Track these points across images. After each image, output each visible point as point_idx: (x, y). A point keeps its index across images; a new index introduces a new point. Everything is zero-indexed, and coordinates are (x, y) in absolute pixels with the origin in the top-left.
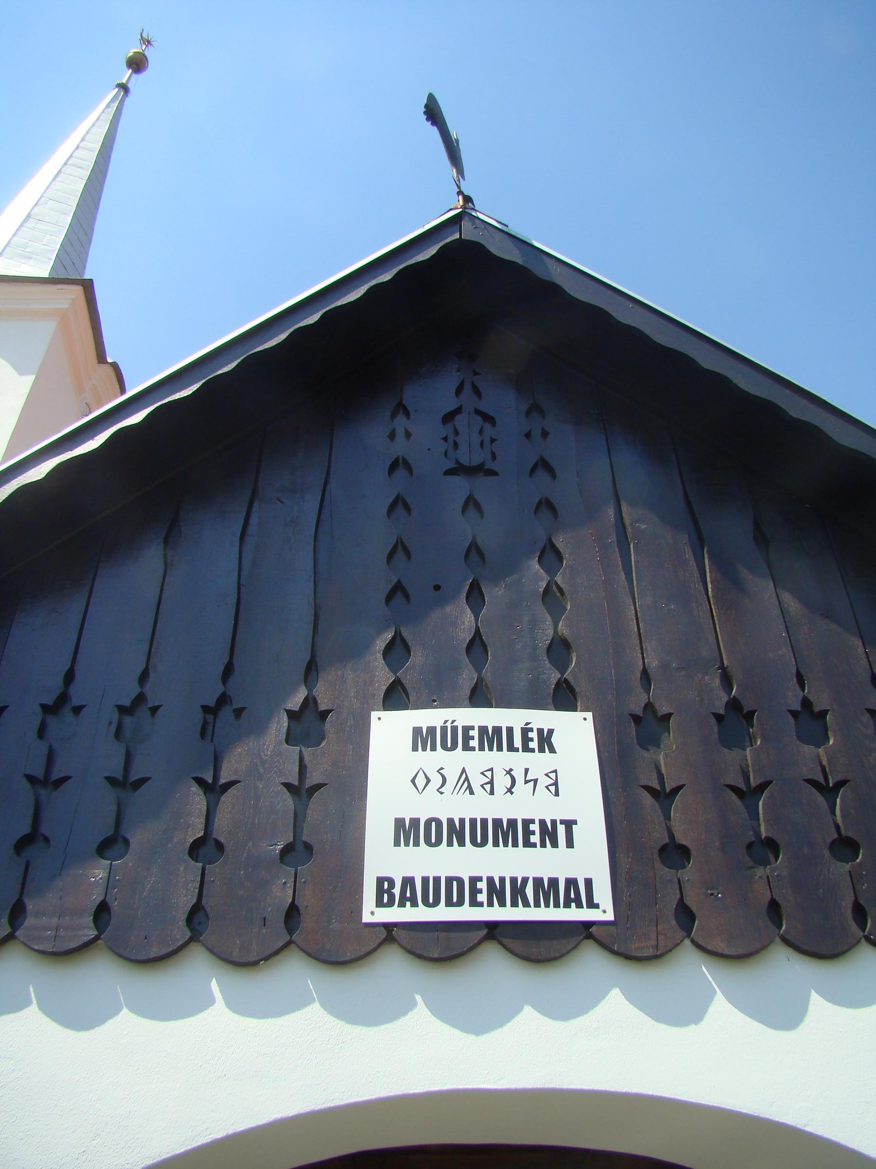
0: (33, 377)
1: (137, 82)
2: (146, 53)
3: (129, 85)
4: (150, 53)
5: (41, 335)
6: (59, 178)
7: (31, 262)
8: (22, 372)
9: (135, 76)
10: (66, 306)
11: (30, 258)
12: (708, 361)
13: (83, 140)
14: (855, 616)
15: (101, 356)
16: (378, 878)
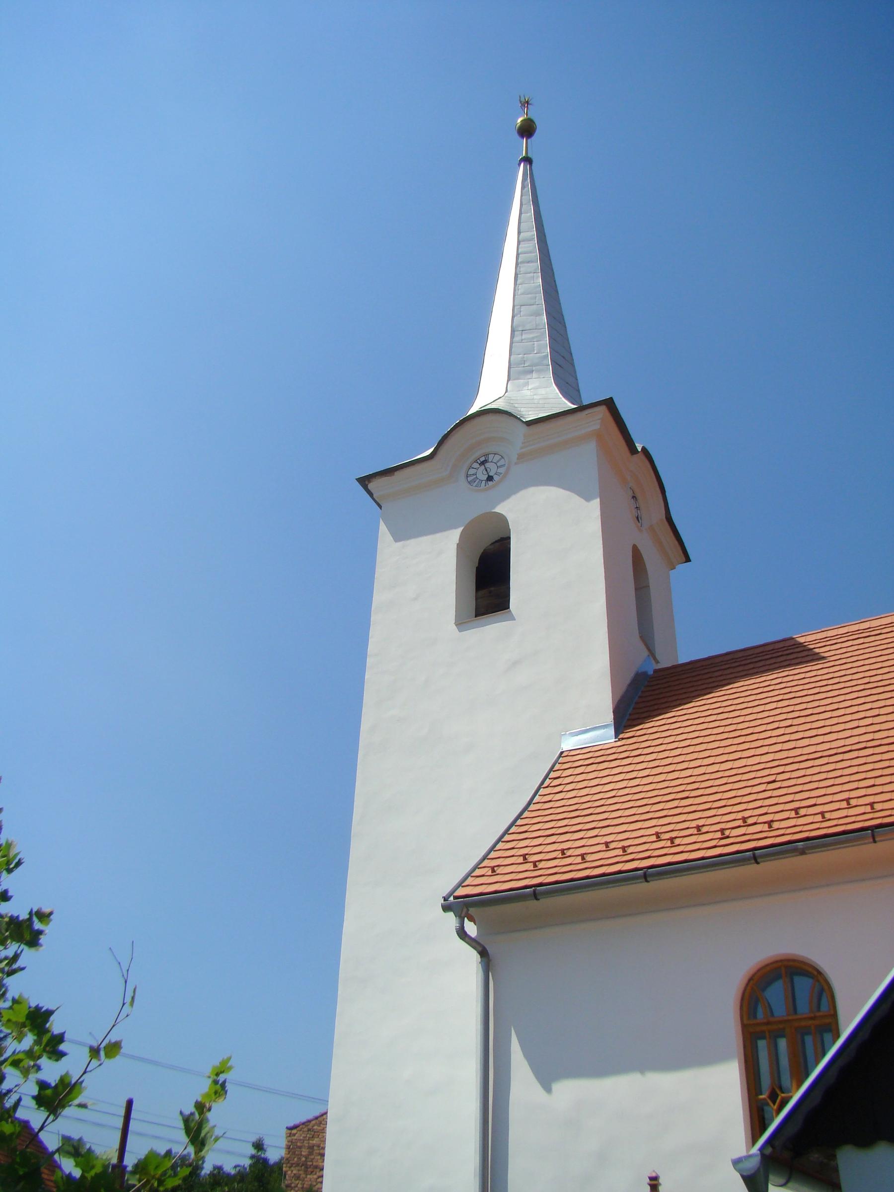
0: (598, 500)
1: (535, 145)
2: (531, 116)
3: (530, 155)
4: (534, 113)
5: (588, 455)
6: (518, 282)
7: (534, 375)
8: (588, 499)
9: (529, 140)
10: (598, 427)
11: (532, 372)
12: (748, 1113)
13: (519, 233)
14: (144, 1121)
15: (633, 449)
16: (611, 398)
